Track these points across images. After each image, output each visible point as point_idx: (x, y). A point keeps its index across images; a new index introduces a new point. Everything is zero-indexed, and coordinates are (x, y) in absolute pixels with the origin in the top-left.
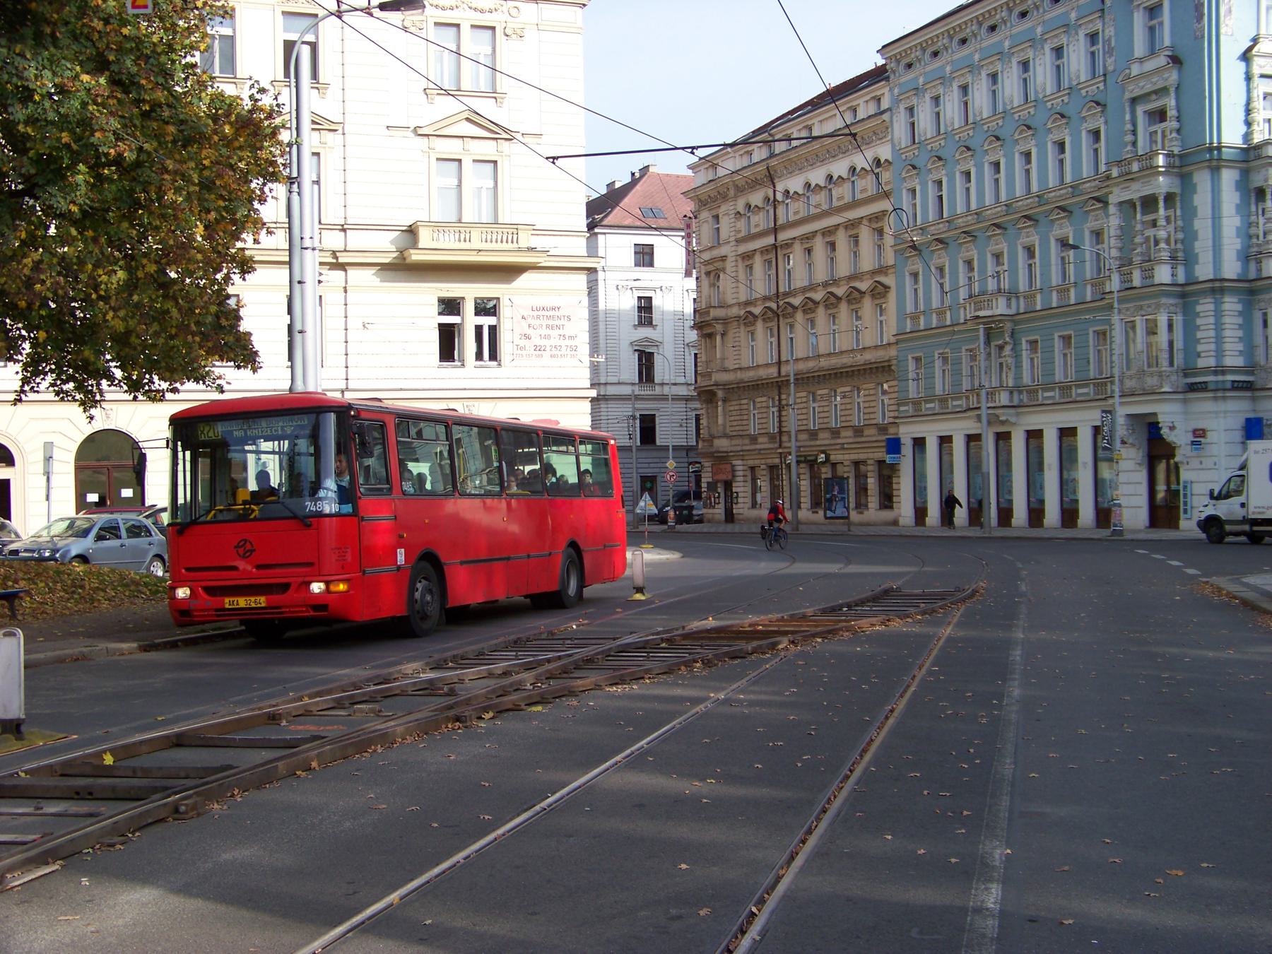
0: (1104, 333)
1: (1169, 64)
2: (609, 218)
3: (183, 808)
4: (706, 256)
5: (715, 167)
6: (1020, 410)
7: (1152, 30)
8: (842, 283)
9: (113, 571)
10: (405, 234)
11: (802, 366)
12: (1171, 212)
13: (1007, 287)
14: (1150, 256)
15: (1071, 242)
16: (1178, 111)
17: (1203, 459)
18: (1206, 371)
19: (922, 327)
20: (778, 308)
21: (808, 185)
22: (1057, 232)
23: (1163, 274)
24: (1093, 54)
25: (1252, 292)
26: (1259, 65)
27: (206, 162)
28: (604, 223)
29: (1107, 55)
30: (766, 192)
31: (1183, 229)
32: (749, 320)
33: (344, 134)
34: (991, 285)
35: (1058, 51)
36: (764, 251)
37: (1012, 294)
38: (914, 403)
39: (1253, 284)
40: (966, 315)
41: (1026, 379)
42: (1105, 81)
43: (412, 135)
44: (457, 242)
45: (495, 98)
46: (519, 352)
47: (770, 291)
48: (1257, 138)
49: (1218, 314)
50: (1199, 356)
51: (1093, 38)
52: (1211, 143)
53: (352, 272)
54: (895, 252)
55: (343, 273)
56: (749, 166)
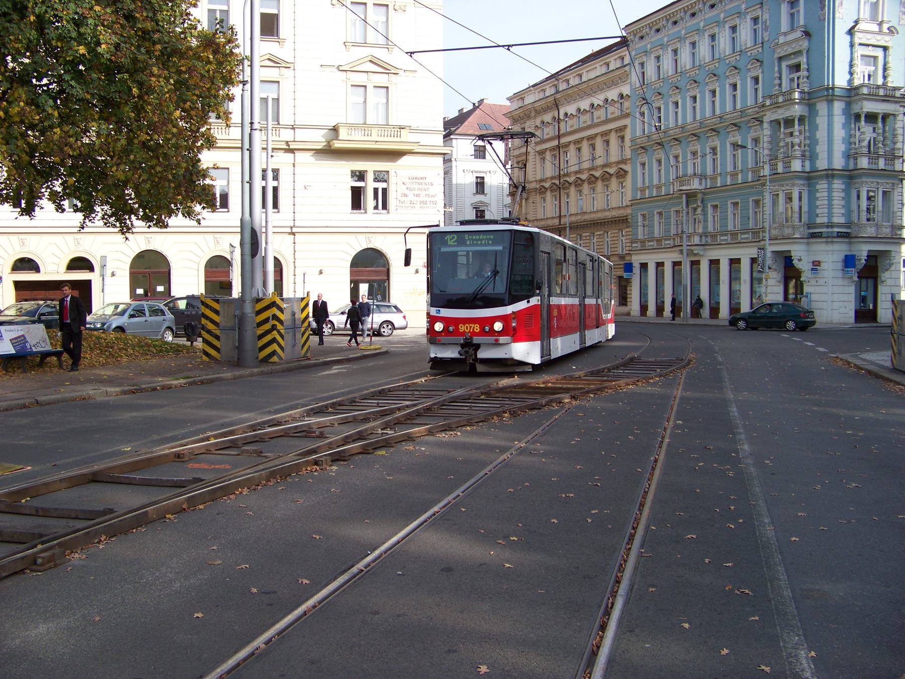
0: (759, 200)
1: (803, 36)
2: (460, 129)
3: (40, 561)
4: (517, 152)
5: (523, 99)
6: (707, 247)
7: (792, 15)
8: (599, 169)
9: (135, 337)
10: (331, 131)
11: (573, 219)
12: (802, 127)
13: (699, 172)
14: (788, 154)
15: (739, 144)
16: (808, 65)
17: (818, 280)
18: (821, 225)
19: (647, 196)
20: (560, 184)
21: (579, 110)
22: (731, 139)
23: (796, 165)
24: (755, 30)
25: (851, 177)
26: (859, 38)
27: (183, 69)
28: (456, 133)
29: (764, 31)
30: (554, 114)
31: (809, 138)
32: (542, 191)
33: (294, 70)
34: (690, 171)
35: (734, 29)
36: (552, 149)
37: (703, 177)
38: (641, 242)
39: (852, 173)
40: (674, 189)
41: (710, 228)
42: (762, 47)
43: (336, 70)
44: (363, 137)
45: (388, 48)
46: (401, 204)
47: (555, 174)
48: (857, 83)
49: (830, 190)
50: (817, 216)
51: (755, 20)
52: (828, 85)
53: (298, 154)
54: (631, 150)
55: (293, 155)
56: (544, 98)
